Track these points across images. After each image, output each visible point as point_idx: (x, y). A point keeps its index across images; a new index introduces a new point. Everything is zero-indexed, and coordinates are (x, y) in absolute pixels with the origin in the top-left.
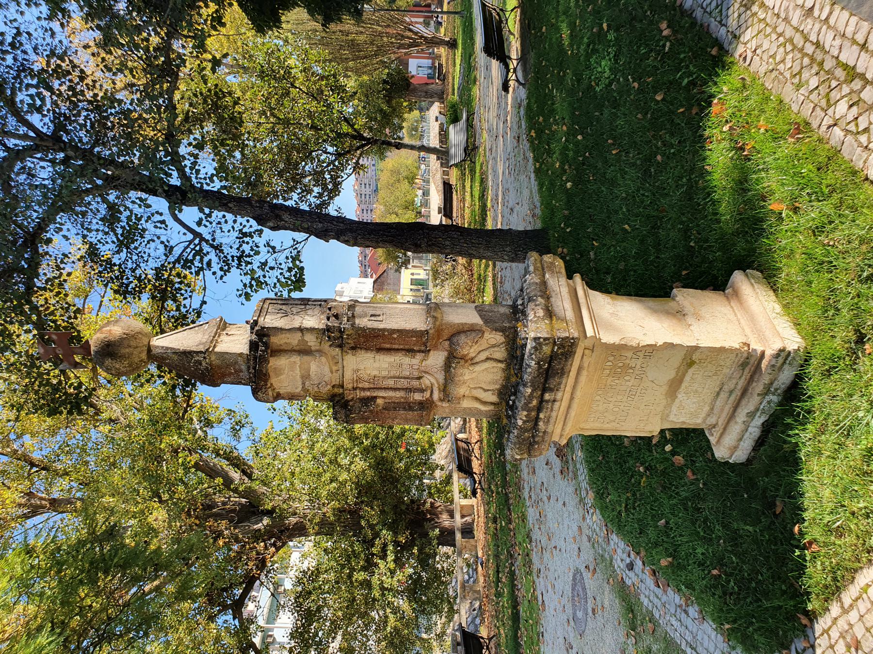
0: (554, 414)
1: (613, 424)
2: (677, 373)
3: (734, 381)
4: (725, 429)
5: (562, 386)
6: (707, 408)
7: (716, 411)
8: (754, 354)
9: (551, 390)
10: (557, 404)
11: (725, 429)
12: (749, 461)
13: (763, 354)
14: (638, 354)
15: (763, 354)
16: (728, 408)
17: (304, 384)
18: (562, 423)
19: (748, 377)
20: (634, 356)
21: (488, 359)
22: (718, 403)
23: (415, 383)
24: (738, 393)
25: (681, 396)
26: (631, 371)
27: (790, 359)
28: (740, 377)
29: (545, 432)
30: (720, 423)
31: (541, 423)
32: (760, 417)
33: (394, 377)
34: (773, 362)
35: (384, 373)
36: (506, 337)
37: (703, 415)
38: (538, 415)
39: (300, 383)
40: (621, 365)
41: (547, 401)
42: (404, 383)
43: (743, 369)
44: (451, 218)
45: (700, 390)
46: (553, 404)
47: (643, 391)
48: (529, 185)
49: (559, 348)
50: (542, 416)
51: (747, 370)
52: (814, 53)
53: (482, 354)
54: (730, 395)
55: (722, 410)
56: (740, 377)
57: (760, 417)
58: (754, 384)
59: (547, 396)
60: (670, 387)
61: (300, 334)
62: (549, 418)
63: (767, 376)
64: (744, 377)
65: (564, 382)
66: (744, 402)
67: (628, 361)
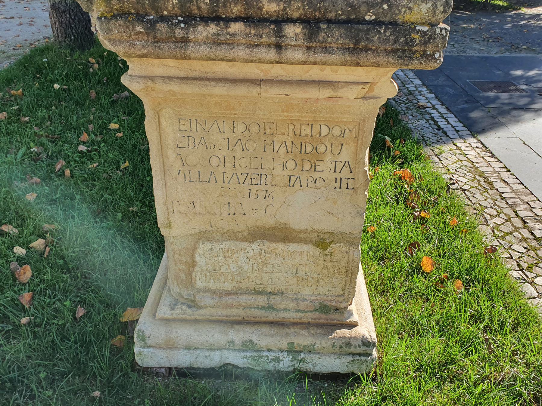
0: (241, 52)
1: (178, 165)
2: (305, 231)
3: (291, 305)
4: (196, 321)
5: (320, 56)
6: (228, 286)
7: (228, 300)
8: (346, 315)
10: (272, 54)
11: (196, 321)
12: (147, 371)
13: (353, 325)
15: (353, 325)
16: (237, 313)
18: (183, 74)
19: (305, 320)
22: (244, 297)
24: (272, 316)
26: (307, 166)
27: (363, 358)
28: (300, 311)
29: (185, 41)
30: (202, 311)
31: (212, 28)
32: (245, 357)
34: (353, 343)
38: (237, 19)
40: (322, 149)
43: (316, 310)
49: (424, 33)
51: (316, 315)
52: (513, 225)
54: (263, 308)
55: (232, 306)
56: (300, 311)
57: (245, 357)
58: (305, 332)
60: (274, 228)
62: (231, 44)
63: (330, 343)
64: (302, 315)
65: (333, 58)
66: (265, 329)
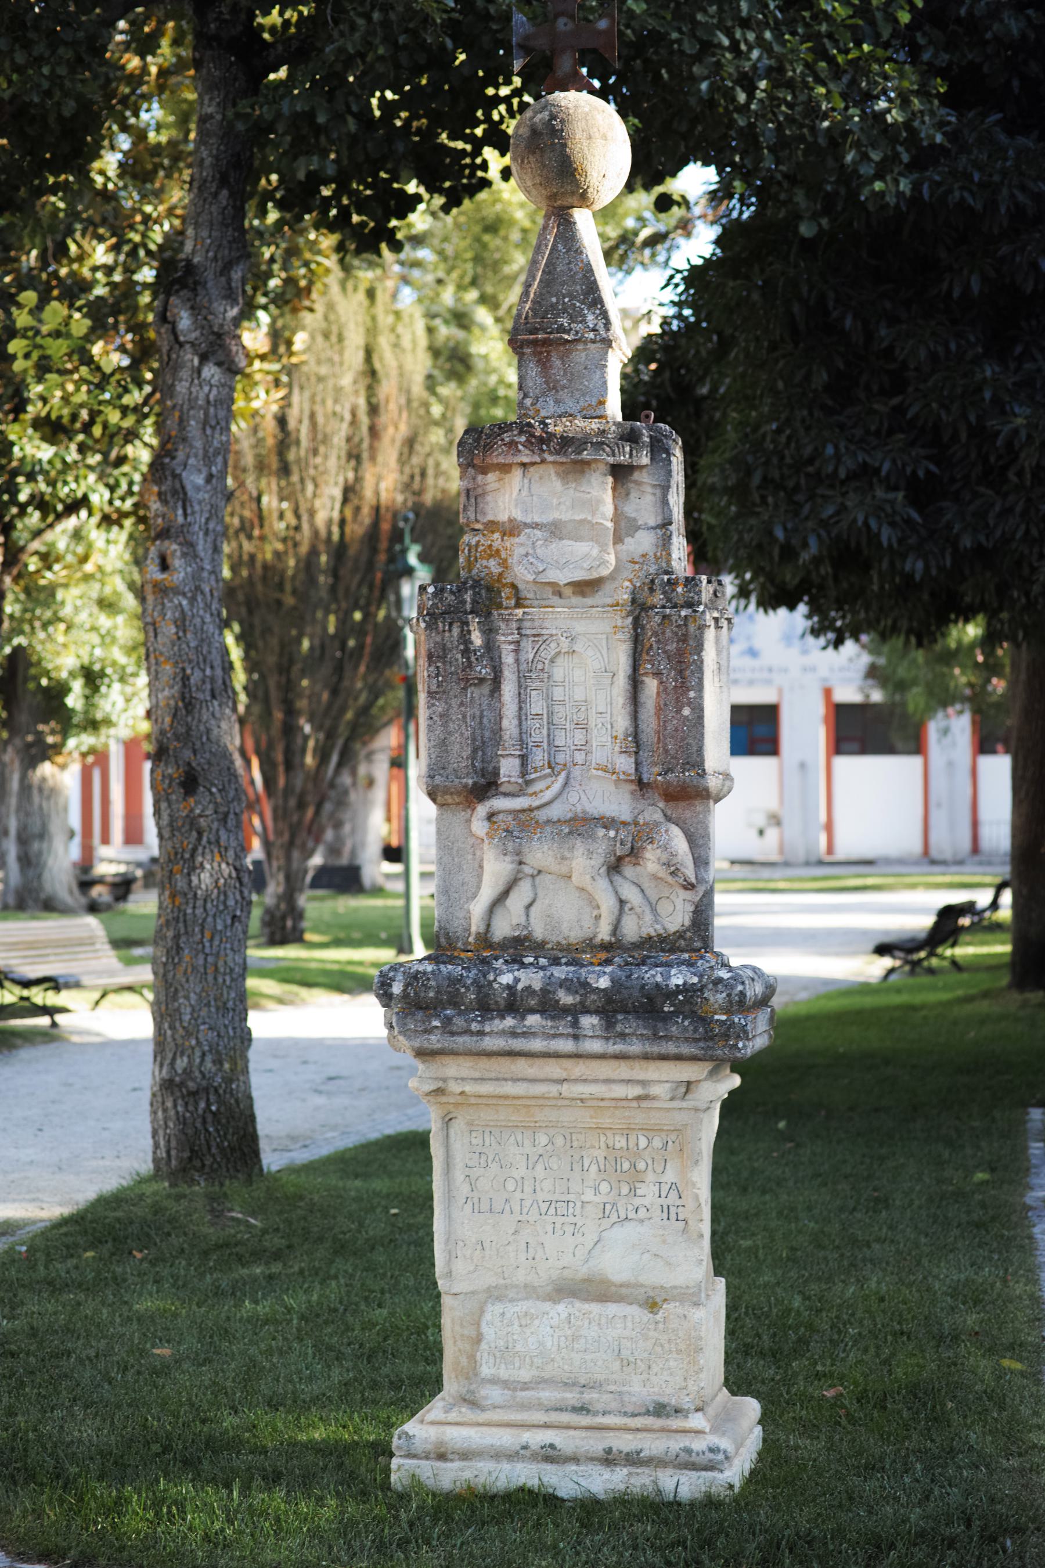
9: (609, 1024)
14: (673, 1194)
17: (536, 526)
20: (665, 1188)
21: (622, 902)
23: (538, 758)
25: (562, 1309)
26: (625, 1190)
33: (551, 714)
35: (558, 693)
36: (680, 935)
37: (503, 1373)
39: (537, 519)
40: (641, 1166)
41: (575, 1024)
42: (538, 734)
44: (315, 884)
45: (580, 1345)
46: (568, 1035)
47: (569, 1229)
48: (294, 1170)
50: (533, 1020)
53: (635, 890)
59: (589, 1022)
61: (652, 522)
67: (650, 1177)
